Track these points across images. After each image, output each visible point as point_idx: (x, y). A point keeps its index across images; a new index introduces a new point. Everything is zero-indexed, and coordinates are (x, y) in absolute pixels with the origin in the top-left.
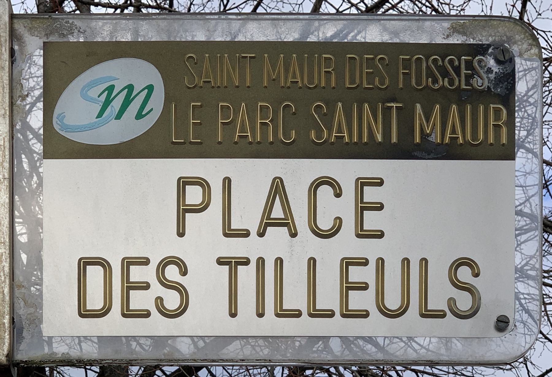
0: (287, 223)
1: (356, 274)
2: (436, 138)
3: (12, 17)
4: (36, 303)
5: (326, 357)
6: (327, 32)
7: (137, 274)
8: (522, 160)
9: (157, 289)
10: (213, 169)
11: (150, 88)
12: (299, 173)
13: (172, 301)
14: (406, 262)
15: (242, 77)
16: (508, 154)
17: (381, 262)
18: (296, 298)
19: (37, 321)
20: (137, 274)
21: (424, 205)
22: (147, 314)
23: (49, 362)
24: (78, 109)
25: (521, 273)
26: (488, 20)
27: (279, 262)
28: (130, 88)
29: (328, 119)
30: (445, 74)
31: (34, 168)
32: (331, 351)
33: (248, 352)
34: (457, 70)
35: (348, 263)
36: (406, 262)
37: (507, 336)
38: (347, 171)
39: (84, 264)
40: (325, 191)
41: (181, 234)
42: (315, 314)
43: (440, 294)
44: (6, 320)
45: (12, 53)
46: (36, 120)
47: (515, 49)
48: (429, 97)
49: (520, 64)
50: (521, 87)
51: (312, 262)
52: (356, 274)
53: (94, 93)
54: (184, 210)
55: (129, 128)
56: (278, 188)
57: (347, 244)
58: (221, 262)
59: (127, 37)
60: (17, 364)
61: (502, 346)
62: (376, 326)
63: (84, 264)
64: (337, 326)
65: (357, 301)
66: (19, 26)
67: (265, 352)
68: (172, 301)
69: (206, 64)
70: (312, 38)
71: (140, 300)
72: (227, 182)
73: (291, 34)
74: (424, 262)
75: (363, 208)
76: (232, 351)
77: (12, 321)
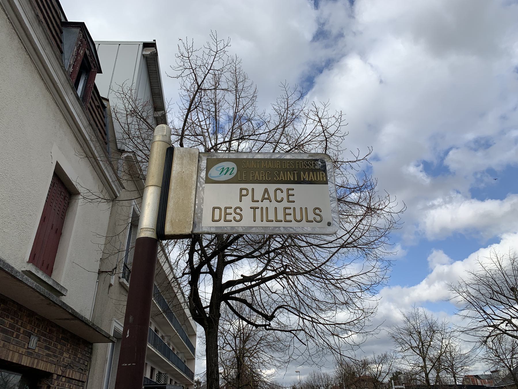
0: (269, 199)
1: (288, 211)
2: (307, 179)
3: (199, 153)
4: (200, 219)
5: (279, 232)
6: (277, 156)
7: (228, 211)
8: (330, 185)
9: (234, 215)
10: (249, 186)
11: (233, 168)
12: (271, 187)
13: (238, 217)
14: (301, 208)
15: (257, 166)
16: (326, 183)
17: (294, 208)
18: (272, 217)
19: (200, 222)
20: (228, 211)
21: (304, 195)
22: (231, 221)
23: (201, 233)
24: (215, 172)
25: (334, 212)
26: (317, 154)
27: (267, 208)
28: (228, 168)
29: (279, 175)
30: (308, 165)
31: (201, 185)
32: (280, 230)
33: (257, 231)
34: (311, 165)
35: (285, 208)
36: (301, 208)
37: (330, 227)
38: (284, 187)
39: (214, 208)
40: (278, 191)
41: (241, 201)
42: (277, 221)
43: (311, 216)
44: (192, 223)
45: (199, 160)
46: (203, 174)
47: (325, 160)
48: (304, 171)
49: (327, 163)
50: (328, 168)
51: (276, 208)
52: (288, 211)
53: (219, 169)
54: (241, 196)
55: (228, 177)
56: (266, 191)
57: (285, 204)
58: (251, 208)
59: (227, 157)
60: (194, 234)
61: (330, 230)
62: (294, 224)
63: (214, 208)
64: (283, 224)
65: (288, 218)
66: (201, 155)
67: (263, 231)
68: (238, 217)
69: (248, 163)
70: (273, 158)
71: (229, 217)
72: (253, 189)
73: (267, 157)
74: (306, 208)
75: (289, 195)
76: (253, 230)
77: (194, 223)
